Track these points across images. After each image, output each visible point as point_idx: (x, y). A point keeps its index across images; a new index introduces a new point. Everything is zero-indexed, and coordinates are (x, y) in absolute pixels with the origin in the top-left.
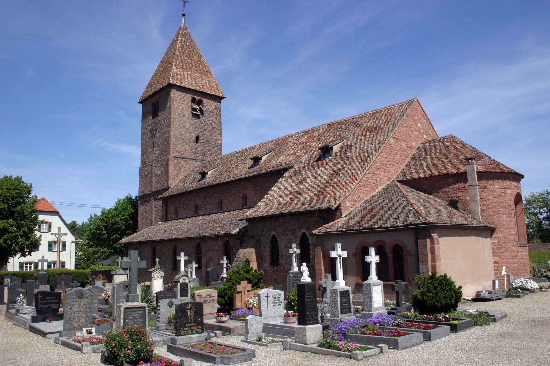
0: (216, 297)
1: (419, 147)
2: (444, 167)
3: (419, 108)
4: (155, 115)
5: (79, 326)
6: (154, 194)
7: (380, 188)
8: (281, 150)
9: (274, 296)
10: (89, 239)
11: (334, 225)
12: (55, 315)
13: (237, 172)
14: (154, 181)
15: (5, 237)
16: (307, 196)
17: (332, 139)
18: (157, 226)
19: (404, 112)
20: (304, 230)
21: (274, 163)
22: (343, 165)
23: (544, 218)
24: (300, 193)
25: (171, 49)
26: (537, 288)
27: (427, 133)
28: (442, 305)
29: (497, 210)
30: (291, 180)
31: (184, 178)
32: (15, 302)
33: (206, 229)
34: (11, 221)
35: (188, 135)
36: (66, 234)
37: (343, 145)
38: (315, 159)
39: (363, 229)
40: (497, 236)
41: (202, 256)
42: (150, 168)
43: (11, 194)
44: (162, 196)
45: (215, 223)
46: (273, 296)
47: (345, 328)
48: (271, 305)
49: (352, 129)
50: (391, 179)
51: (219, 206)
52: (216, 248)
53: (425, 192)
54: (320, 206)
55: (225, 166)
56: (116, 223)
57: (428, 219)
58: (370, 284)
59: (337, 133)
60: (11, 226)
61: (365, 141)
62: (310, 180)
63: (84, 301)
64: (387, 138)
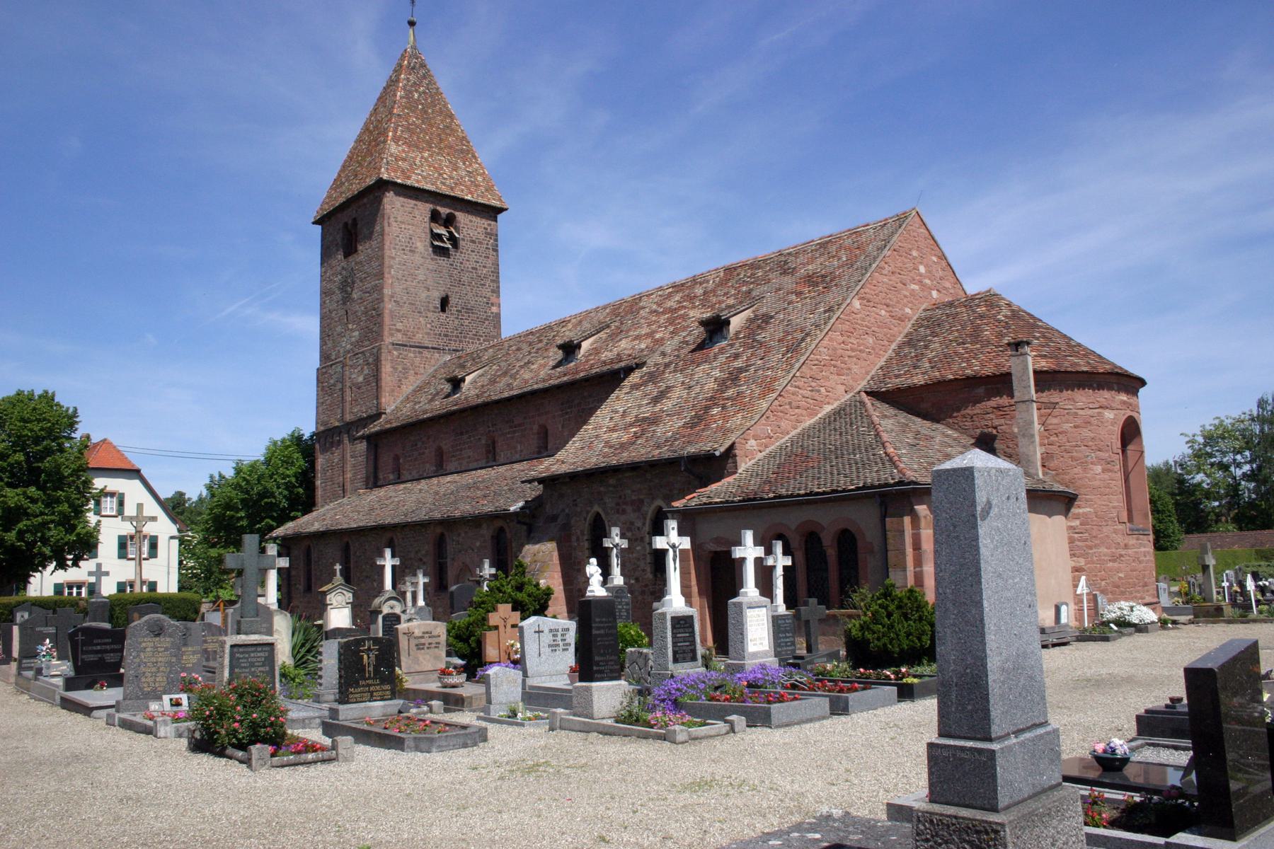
0: (444, 637)
1: (920, 318)
3: (923, 230)
4: (350, 250)
5: (155, 690)
6: (349, 428)
7: (828, 409)
8: (624, 328)
9: (553, 632)
10: (207, 530)
11: (719, 491)
12: (111, 677)
13: (527, 376)
14: (348, 399)
15: (21, 525)
16: (669, 427)
17: (731, 301)
18: (354, 498)
19: (887, 241)
20: (659, 502)
21: (606, 355)
23: (1244, 474)
24: (654, 420)
25: (384, 102)
26: (1153, 622)
27: (939, 287)
28: (902, 650)
29: (1079, 455)
30: (638, 393)
31: (414, 391)
32: (36, 655)
33: (455, 502)
34: (32, 490)
35: (424, 295)
36: (154, 519)
37: (752, 316)
38: (692, 347)
39: (775, 498)
40: (1081, 511)
42: (339, 369)
43: (31, 430)
44: (366, 431)
45: (478, 488)
46: (551, 631)
47: (678, 689)
49: (776, 279)
50: (852, 388)
51: (488, 452)
52: (478, 544)
53: (925, 416)
54: (692, 449)
55: (502, 364)
56: (266, 493)
57: (909, 473)
58: (740, 604)
59: (744, 289)
60: (34, 501)
62: (677, 393)
63: (165, 641)
64: (844, 299)
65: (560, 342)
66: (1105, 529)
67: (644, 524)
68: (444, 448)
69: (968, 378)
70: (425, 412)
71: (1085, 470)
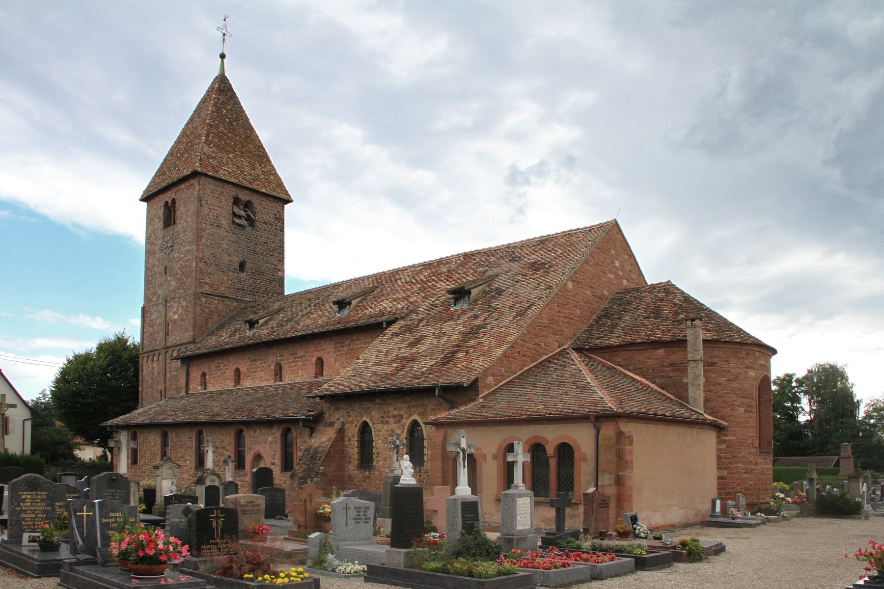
0: (263, 506)
2: (651, 330)
8: (385, 292)
9: (358, 509)
13: (308, 322)
22: (485, 319)
24: (412, 359)
25: (199, 114)
30: (397, 339)
35: (226, 259)
36: (14, 406)
40: (727, 438)
41: (246, 449)
46: (356, 508)
48: (351, 522)
49: (506, 265)
51: (276, 375)
52: (270, 439)
59: (480, 270)
61: (525, 283)
62: (429, 341)
67: (403, 432)
68: (241, 369)
70: (227, 343)
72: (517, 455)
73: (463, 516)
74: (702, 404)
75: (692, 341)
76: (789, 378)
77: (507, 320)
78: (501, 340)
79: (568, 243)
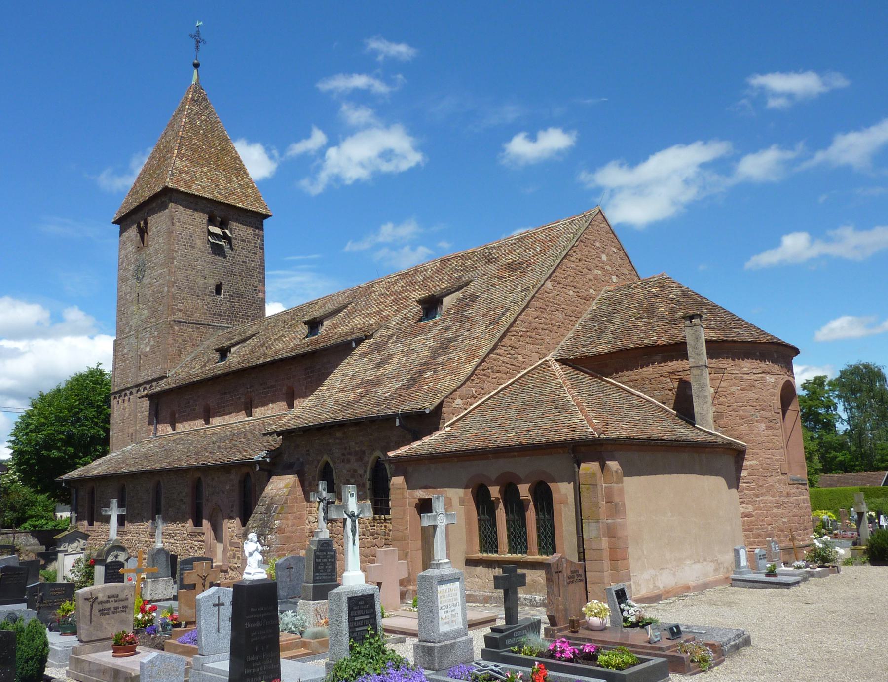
2: (645, 333)
8: (358, 307)
13: (280, 346)
20: (378, 453)
21: (342, 329)
22: (457, 330)
24: (377, 382)
25: (172, 127)
29: (746, 414)
30: (364, 360)
52: (228, 488)
54: (406, 407)
59: (456, 275)
65: (307, 318)
66: (769, 479)
67: (365, 472)
69: (647, 346)
71: (751, 426)
72: (435, 517)
73: (351, 619)
74: (711, 421)
75: (692, 343)
76: (819, 381)
77: (479, 330)
78: (472, 355)
79: (548, 238)
